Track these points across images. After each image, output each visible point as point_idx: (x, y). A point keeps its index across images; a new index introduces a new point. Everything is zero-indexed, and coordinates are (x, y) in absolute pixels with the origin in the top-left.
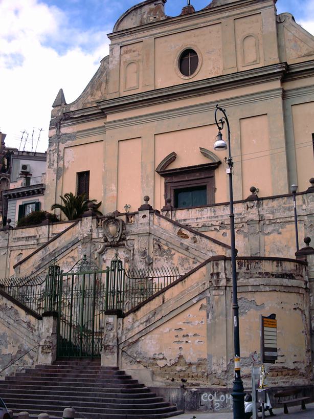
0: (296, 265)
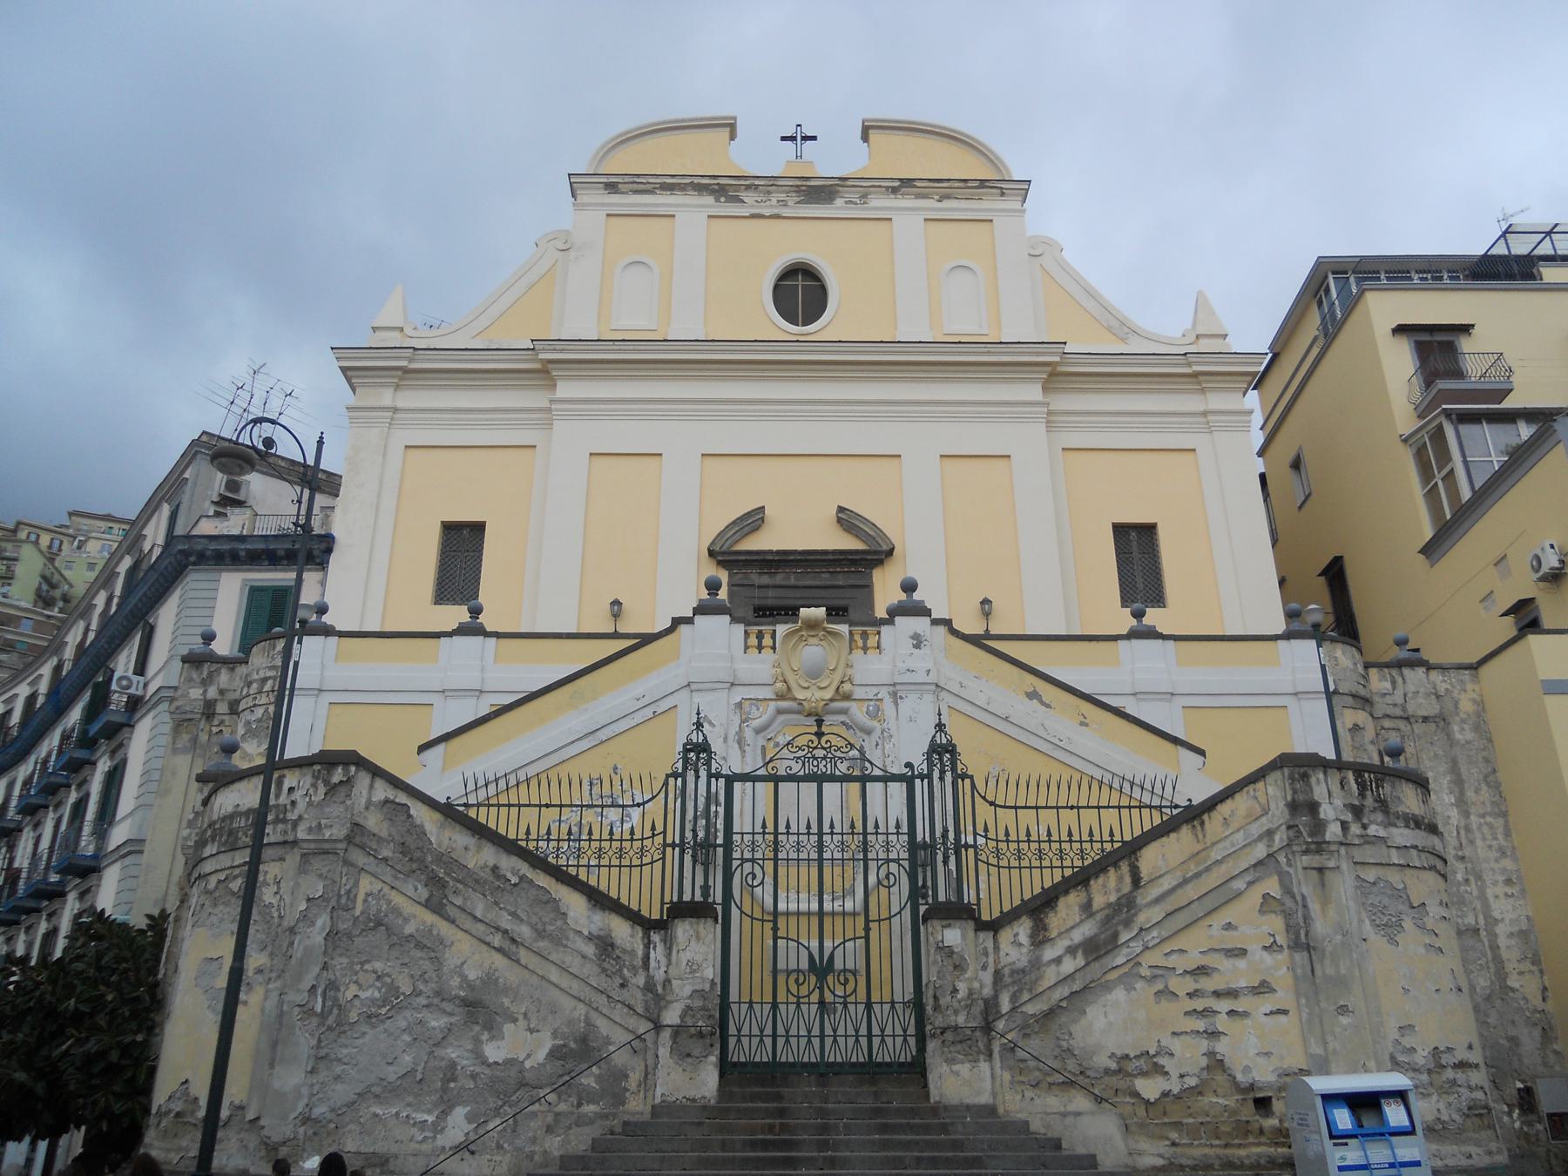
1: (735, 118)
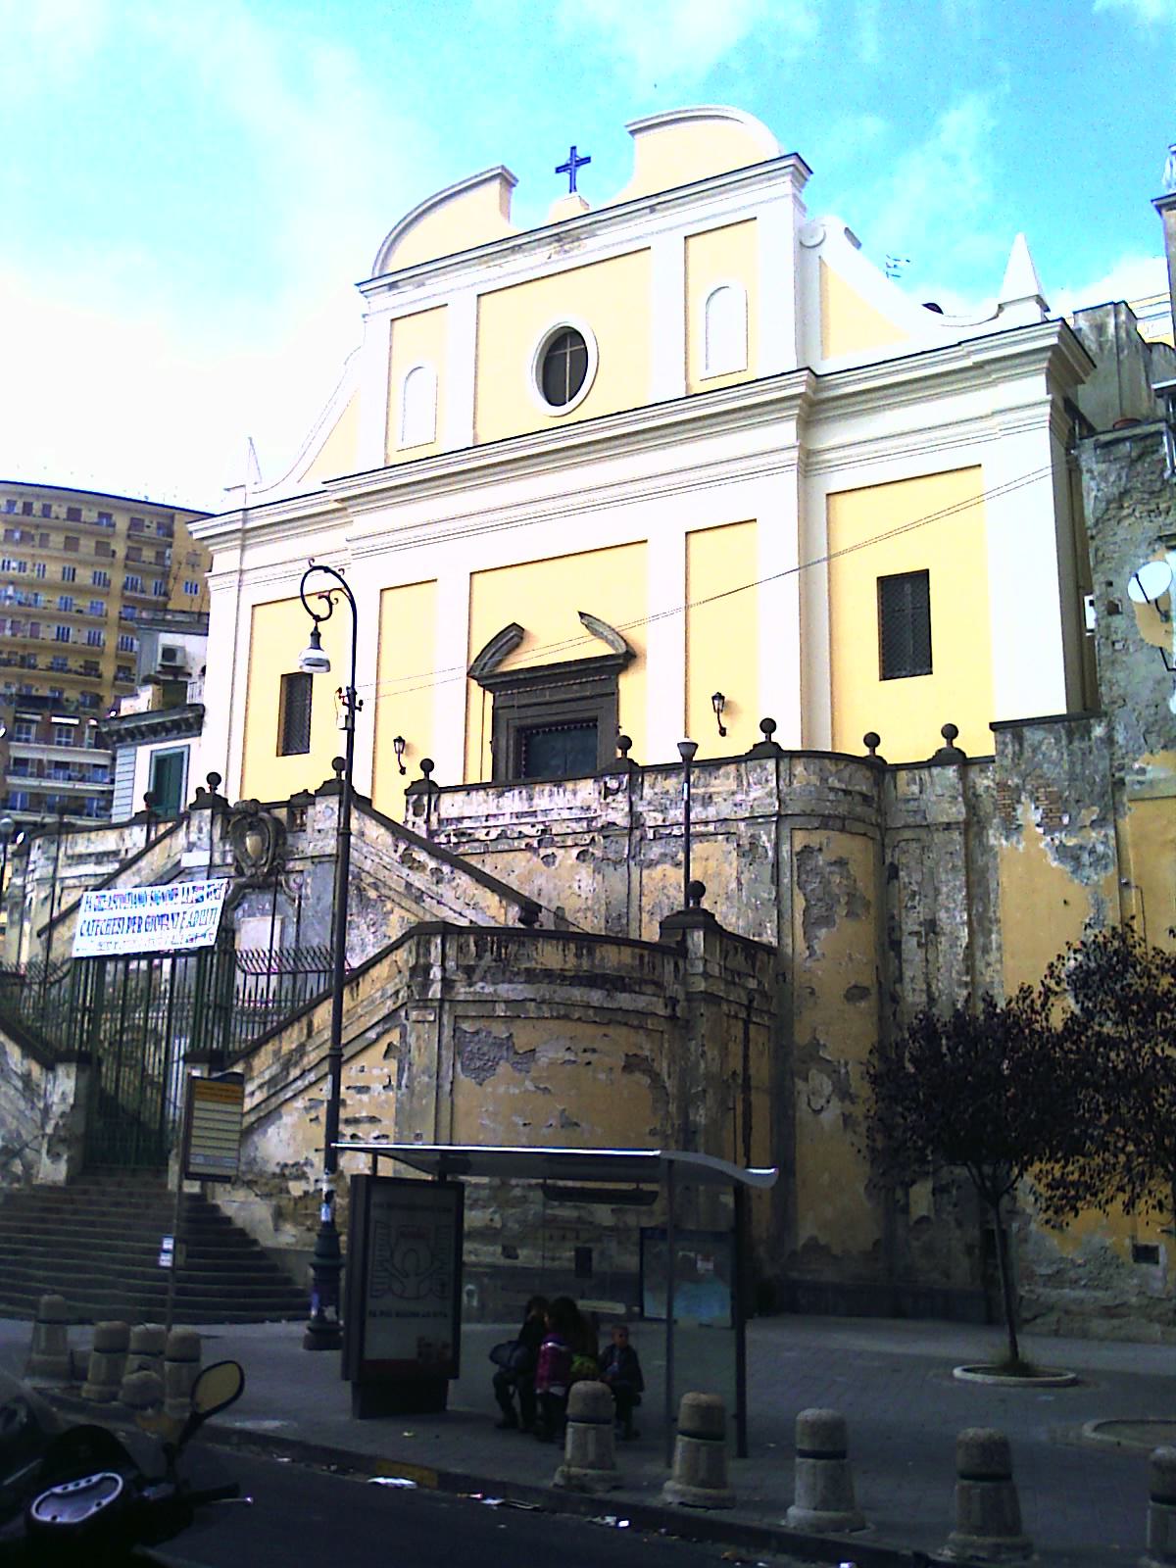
0: (642, 957)
1: (517, 181)
